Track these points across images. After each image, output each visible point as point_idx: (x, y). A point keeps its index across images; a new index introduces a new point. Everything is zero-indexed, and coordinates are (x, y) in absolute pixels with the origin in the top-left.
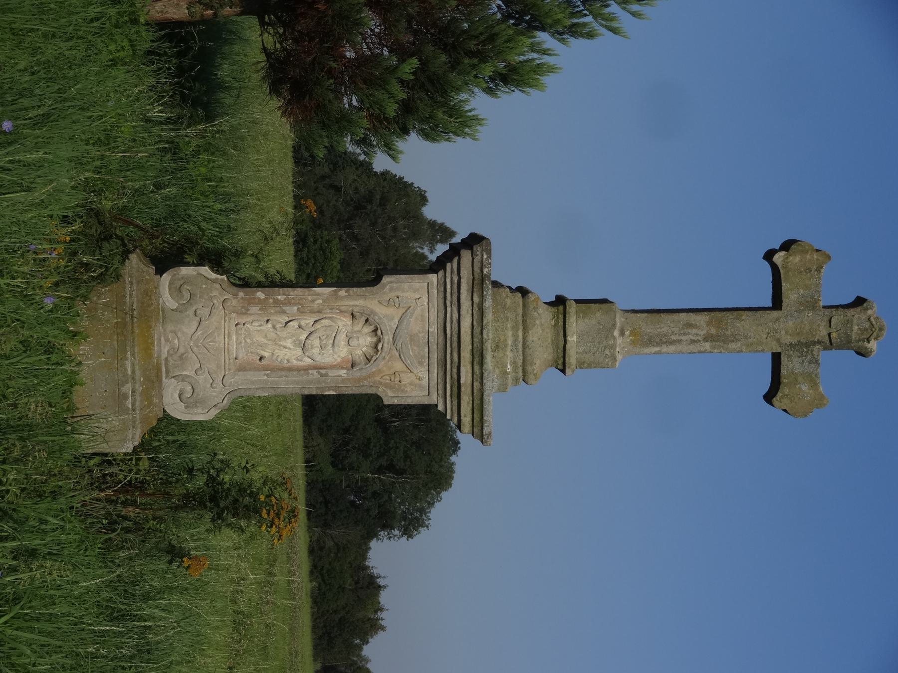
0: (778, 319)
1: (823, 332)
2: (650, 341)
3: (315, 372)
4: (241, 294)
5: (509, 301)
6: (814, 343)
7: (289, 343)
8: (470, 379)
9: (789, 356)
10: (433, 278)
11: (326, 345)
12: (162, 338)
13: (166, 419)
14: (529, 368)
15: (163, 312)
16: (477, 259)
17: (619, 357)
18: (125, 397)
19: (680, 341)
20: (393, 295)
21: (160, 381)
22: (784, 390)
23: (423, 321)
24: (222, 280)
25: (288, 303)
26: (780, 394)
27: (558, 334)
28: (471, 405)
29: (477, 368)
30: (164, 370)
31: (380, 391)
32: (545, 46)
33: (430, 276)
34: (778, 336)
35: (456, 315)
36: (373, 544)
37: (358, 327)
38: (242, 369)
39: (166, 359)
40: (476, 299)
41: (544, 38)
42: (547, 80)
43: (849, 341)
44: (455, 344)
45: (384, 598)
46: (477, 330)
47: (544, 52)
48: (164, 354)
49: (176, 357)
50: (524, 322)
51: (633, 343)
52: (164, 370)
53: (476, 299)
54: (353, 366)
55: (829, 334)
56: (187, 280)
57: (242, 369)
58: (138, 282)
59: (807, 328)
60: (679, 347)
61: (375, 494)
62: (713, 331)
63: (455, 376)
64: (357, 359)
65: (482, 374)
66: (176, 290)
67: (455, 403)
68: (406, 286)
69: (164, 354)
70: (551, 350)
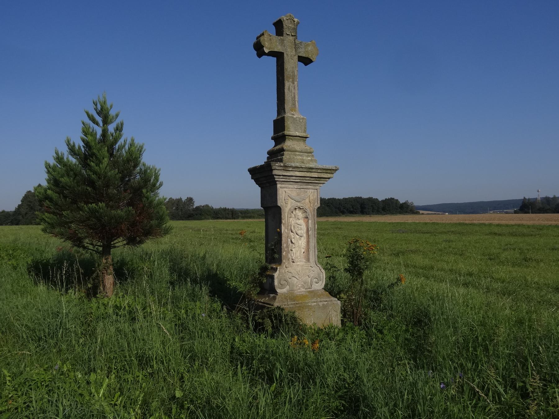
0: (287, 55)
1: (291, 38)
2: (294, 104)
5: (288, 157)
6: (295, 42)
7: (300, 242)
10: (279, 186)
13: (326, 288)
14: (309, 151)
16: (277, 168)
17: (302, 117)
18: (323, 305)
19: (294, 93)
21: (313, 291)
22: (310, 56)
25: (287, 243)
27: (295, 140)
29: (313, 171)
31: (316, 208)
32: (123, 142)
35: (294, 178)
37: (293, 215)
38: (308, 260)
40: (291, 169)
44: (303, 178)
46: (301, 170)
48: (304, 290)
53: (291, 169)
56: (279, 282)
60: (296, 94)
62: (291, 80)
65: (330, 170)
66: (282, 286)
68: (281, 197)
69: (304, 290)
70: (300, 142)
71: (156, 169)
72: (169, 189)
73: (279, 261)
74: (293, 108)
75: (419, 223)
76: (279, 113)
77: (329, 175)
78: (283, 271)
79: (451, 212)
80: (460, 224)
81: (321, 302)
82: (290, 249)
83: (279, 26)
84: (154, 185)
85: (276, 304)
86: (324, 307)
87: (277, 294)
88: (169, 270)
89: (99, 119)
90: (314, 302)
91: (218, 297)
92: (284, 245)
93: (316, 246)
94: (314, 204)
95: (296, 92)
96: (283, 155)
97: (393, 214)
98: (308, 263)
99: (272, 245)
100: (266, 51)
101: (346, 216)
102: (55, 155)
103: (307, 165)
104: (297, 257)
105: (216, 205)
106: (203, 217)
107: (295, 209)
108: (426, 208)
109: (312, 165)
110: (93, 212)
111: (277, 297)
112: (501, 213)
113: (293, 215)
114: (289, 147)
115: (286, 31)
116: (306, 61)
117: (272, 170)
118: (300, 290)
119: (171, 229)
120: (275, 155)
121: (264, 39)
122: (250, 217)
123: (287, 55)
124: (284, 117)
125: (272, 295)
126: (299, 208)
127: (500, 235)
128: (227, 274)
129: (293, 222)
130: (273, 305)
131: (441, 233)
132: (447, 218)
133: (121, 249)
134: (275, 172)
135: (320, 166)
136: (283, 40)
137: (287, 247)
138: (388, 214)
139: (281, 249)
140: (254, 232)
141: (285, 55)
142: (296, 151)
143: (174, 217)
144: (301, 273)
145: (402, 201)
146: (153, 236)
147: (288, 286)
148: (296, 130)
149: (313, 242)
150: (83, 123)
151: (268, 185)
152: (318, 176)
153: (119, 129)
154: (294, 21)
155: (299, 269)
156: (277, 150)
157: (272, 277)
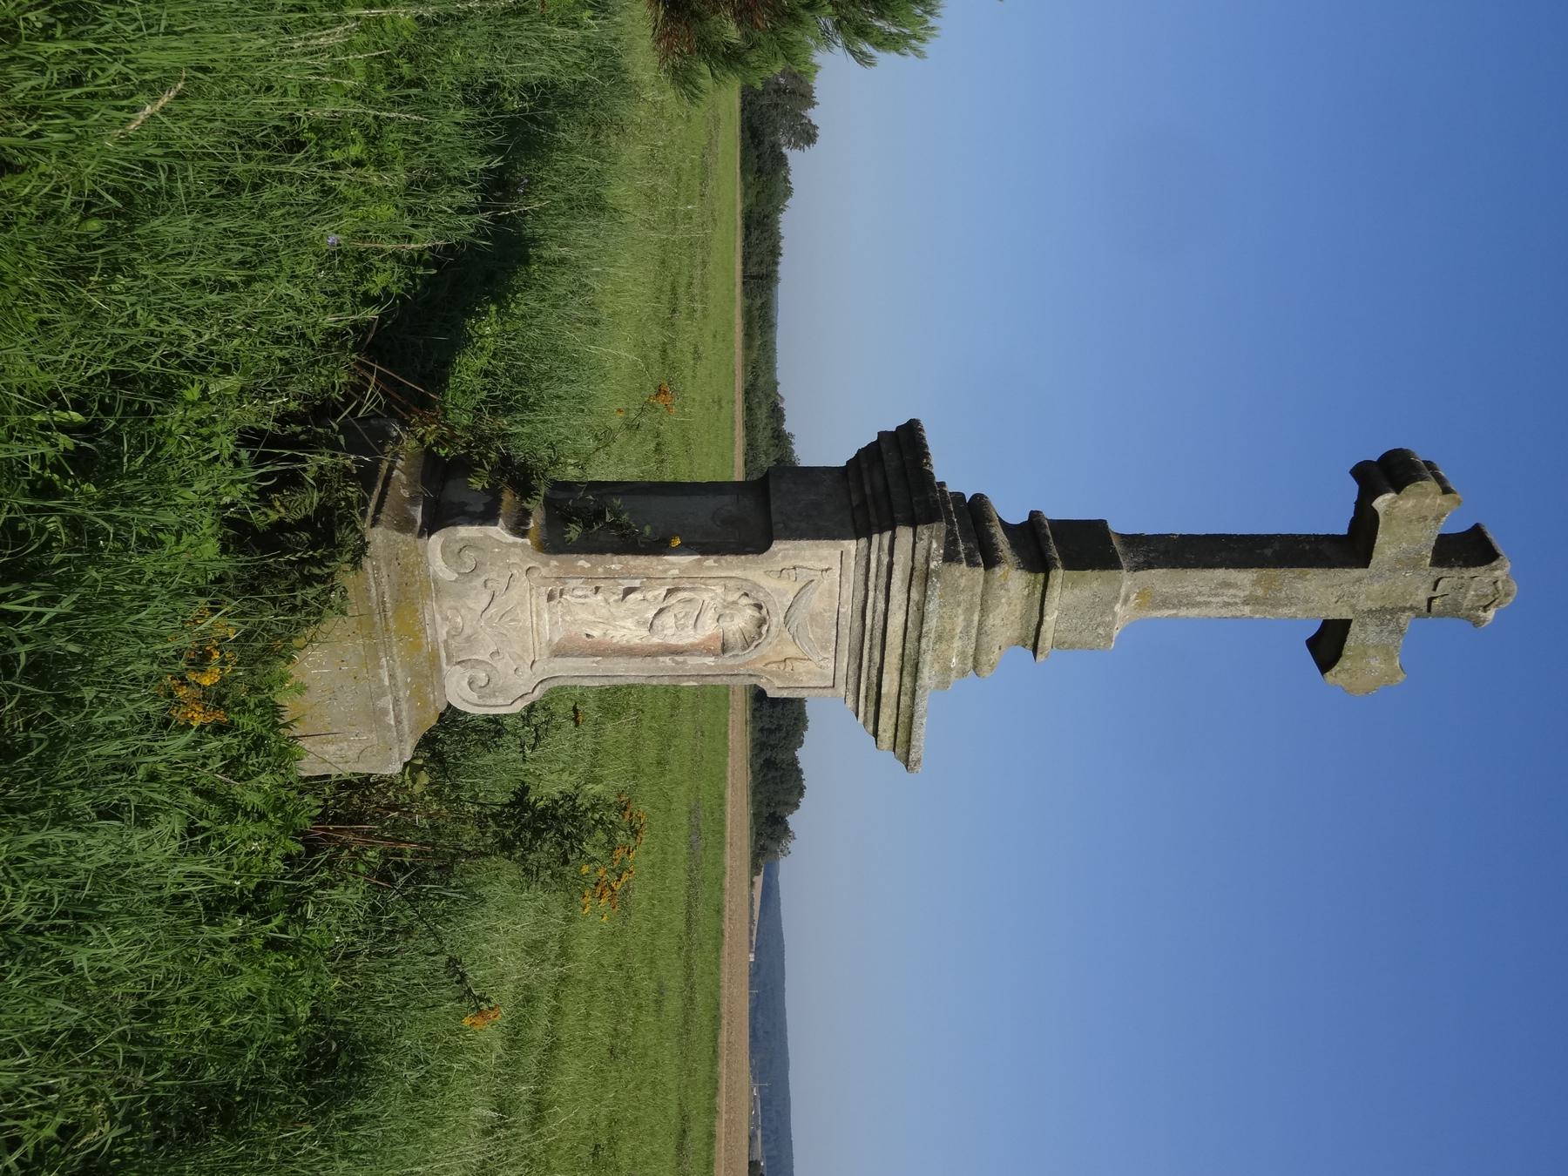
0: (1359, 580)
1: (1422, 596)
2: (1165, 603)
3: (667, 659)
4: (554, 563)
5: (963, 582)
6: (1403, 610)
7: (629, 623)
9: (1363, 625)
10: (851, 546)
12: (438, 617)
13: (450, 718)
14: (983, 659)
15: (436, 583)
16: (921, 545)
17: (1116, 633)
18: (385, 712)
19: (1207, 604)
21: (440, 670)
22: (1344, 663)
23: (830, 597)
24: (524, 545)
26: (1337, 668)
27: (1029, 608)
28: (894, 720)
29: (907, 680)
30: (443, 654)
33: (846, 542)
34: (1354, 601)
35: (881, 606)
37: (734, 596)
38: (559, 652)
39: (446, 642)
40: (915, 595)
44: (877, 641)
46: (912, 634)
48: (442, 635)
52: (443, 654)
54: (724, 648)
55: (1430, 600)
56: (469, 545)
57: (559, 652)
58: (389, 564)
59: (1399, 591)
60: (1205, 611)
62: (1260, 592)
63: (875, 679)
65: (909, 741)
66: (454, 555)
67: (872, 709)
68: (808, 553)
69: (442, 635)
70: (1017, 626)
71: (922, 40)
72: (839, 79)
73: (552, 544)
75: (722, 890)
76: (1132, 541)
77: (890, 733)
79: (756, 970)
80: (716, 1018)
81: (396, 701)
82: (601, 584)
83: (1466, 548)
84: (862, 32)
85: (378, 537)
86: (377, 716)
87: (421, 535)
88: (542, 83)
90: (392, 676)
91: (428, 282)
92: (616, 563)
93: (615, 681)
94: (778, 676)
95: (1212, 612)
96: (972, 563)
97: (754, 793)
98: (546, 653)
99: (617, 514)
100: (1381, 503)
103: (927, 658)
104: (569, 612)
105: (791, 223)
106: (750, 178)
107: (759, 607)
108: (770, 894)
109: (928, 675)
111: (410, 537)
112: (753, 1119)
113: (734, 596)
114: (1002, 586)
115: (1451, 577)
116: (1328, 644)
117: (913, 523)
119: (693, 97)
120: (971, 530)
121: (1426, 495)
122: (748, 335)
123: (1359, 580)
124: (1118, 566)
125: (418, 513)
126: (761, 622)
127: (680, 1148)
128: (526, 302)
129: (706, 596)
130: (375, 522)
131: (689, 968)
132: (738, 958)
135: (923, 705)
138: (754, 778)
139: (601, 551)
140: (697, 356)
142: (984, 610)
143: (749, 99)
144: (505, 623)
145: (793, 820)
146: (665, 25)
147: (454, 576)
148: (1065, 612)
149: (627, 671)
151: (855, 499)
152: (889, 712)
154: (1485, 608)
155: (525, 618)
156: (992, 536)
157: (488, 516)
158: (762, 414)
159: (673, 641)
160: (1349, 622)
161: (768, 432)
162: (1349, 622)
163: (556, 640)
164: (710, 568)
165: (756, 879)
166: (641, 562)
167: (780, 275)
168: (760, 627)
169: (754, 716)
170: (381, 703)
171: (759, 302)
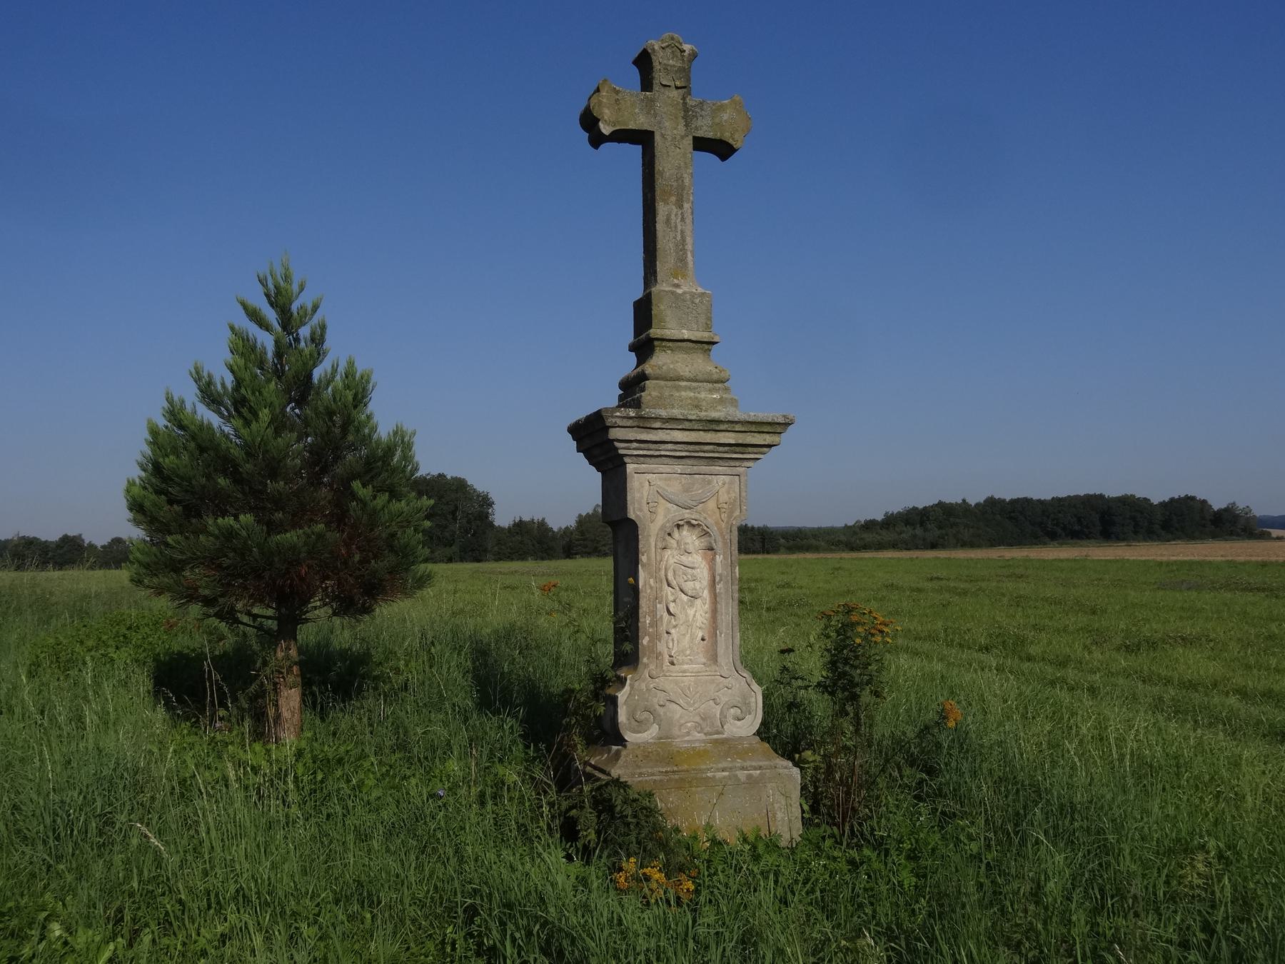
0: (663, 136)
1: (675, 94)
2: (682, 260)
4: (645, 660)
5: (654, 394)
6: (685, 104)
7: (691, 612)
8: (733, 435)
9: (696, 128)
10: (630, 468)
11: (693, 575)
13: (763, 733)
14: (715, 377)
16: (619, 422)
17: (700, 290)
18: (749, 777)
19: (682, 232)
20: (645, 508)
22: (726, 136)
25: (653, 613)
26: (731, 141)
29: (722, 427)
30: (715, 736)
32: (329, 370)
35: (670, 446)
36: (496, 524)
37: (673, 543)
38: (714, 658)
40: (658, 425)
41: (317, 374)
42: (360, 368)
43: (682, 70)
44: (697, 448)
45: (526, 518)
46: (687, 425)
47: (334, 370)
49: (704, 725)
50: (672, 379)
51: (684, 276)
52: (715, 736)
53: (658, 425)
54: (711, 549)
55: (677, 88)
56: (632, 715)
57: (714, 658)
58: (639, 767)
60: (688, 233)
61: (469, 522)
62: (673, 199)
64: (704, 545)
66: (640, 726)
67: (750, 449)
68: (637, 495)
74: (680, 269)
78: (643, 686)
81: (743, 768)
87: (625, 746)
89: (271, 315)
92: (645, 620)
94: (731, 512)
95: (688, 229)
98: (714, 667)
100: (606, 129)
101: (1061, 545)
102: (166, 405)
110: (230, 534)
111: (624, 753)
115: (660, 77)
117: (606, 429)
118: (689, 734)
121: (600, 103)
122: (808, 549)
123: (663, 136)
125: (615, 748)
126: (688, 523)
129: (671, 561)
133: (322, 624)
134: (614, 434)
135: (739, 415)
136: (652, 101)
137: (655, 623)
138: (1179, 538)
141: (657, 137)
142: (679, 379)
145: (1217, 504)
147: (656, 726)
149: (729, 611)
150: (232, 328)
152: (746, 441)
153: (318, 339)
157: (613, 701)
158: (869, 537)
159: (705, 583)
160: (694, 138)
161: (884, 532)
162: (694, 138)
163: (704, 660)
164: (649, 558)
165: (1274, 535)
166: (643, 603)
167: (761, 525)
168: (694, 526)
169: (1124, 540)
170: (743, 779)
171: (782, 541)
